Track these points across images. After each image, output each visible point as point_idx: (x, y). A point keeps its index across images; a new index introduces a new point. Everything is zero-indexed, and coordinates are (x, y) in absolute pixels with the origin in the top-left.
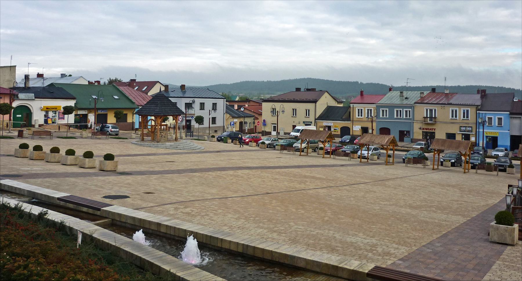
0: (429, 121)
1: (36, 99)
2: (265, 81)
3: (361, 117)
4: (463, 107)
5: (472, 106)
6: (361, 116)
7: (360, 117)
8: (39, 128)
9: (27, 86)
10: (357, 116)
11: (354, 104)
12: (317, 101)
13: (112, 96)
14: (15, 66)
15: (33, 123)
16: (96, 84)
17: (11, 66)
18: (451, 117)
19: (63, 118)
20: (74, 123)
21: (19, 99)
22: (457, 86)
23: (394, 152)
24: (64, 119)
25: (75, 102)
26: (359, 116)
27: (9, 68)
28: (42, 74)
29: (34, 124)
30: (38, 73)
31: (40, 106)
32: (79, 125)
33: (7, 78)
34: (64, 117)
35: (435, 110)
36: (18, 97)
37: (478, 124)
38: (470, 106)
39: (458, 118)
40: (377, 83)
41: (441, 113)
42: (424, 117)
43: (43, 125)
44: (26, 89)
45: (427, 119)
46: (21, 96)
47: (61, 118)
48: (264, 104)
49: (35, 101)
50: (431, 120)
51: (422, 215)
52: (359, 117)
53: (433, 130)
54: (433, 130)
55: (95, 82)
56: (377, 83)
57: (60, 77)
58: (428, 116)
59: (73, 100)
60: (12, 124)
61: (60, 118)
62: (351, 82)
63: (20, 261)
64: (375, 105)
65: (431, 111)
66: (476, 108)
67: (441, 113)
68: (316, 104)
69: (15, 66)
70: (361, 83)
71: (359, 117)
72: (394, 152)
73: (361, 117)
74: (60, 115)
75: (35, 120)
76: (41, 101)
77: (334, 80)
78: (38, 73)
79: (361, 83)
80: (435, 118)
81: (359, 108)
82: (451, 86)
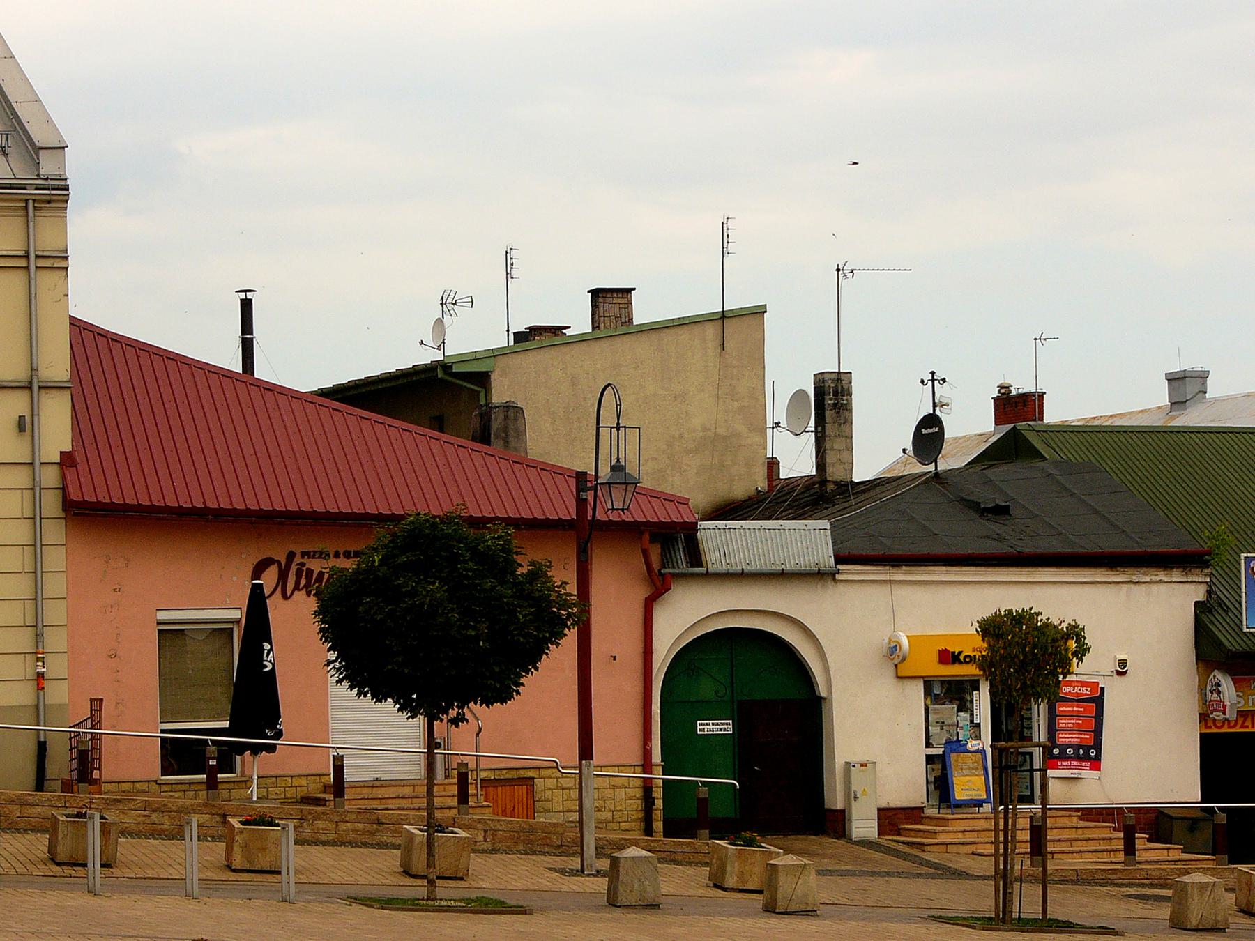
1: (850, 572)
8: (887, 840)
9: (835, 473)
14: (760, 311)
15: (835, 798)
17: (723, 316)
19: (1086, 758)
20: (1199, 800)
21: (708, 575)
23: (1037, 770)
24: (1096, 764)
25: (1199, 593)
27: (711, 331)
28: (1028, 388)
29: (840, 806)
30: (1004, 388)
31: (881, 638)
32: (1222, 819)
33: (697, 422)
34: (1098, 746)
36: (695, 556)
43: (914, 813)
47: (1077, 747)
49: (841, 588)
51: (555, 460)
57: (1166, 402)
59: (1176, 576)
60: (659, 803)
61: (1064, 748)
69: (760, 311)
72: (1037, 770)
74: (1062, 723)
75: (848, 766)
76: (886, 589)
78: (1004, 388)
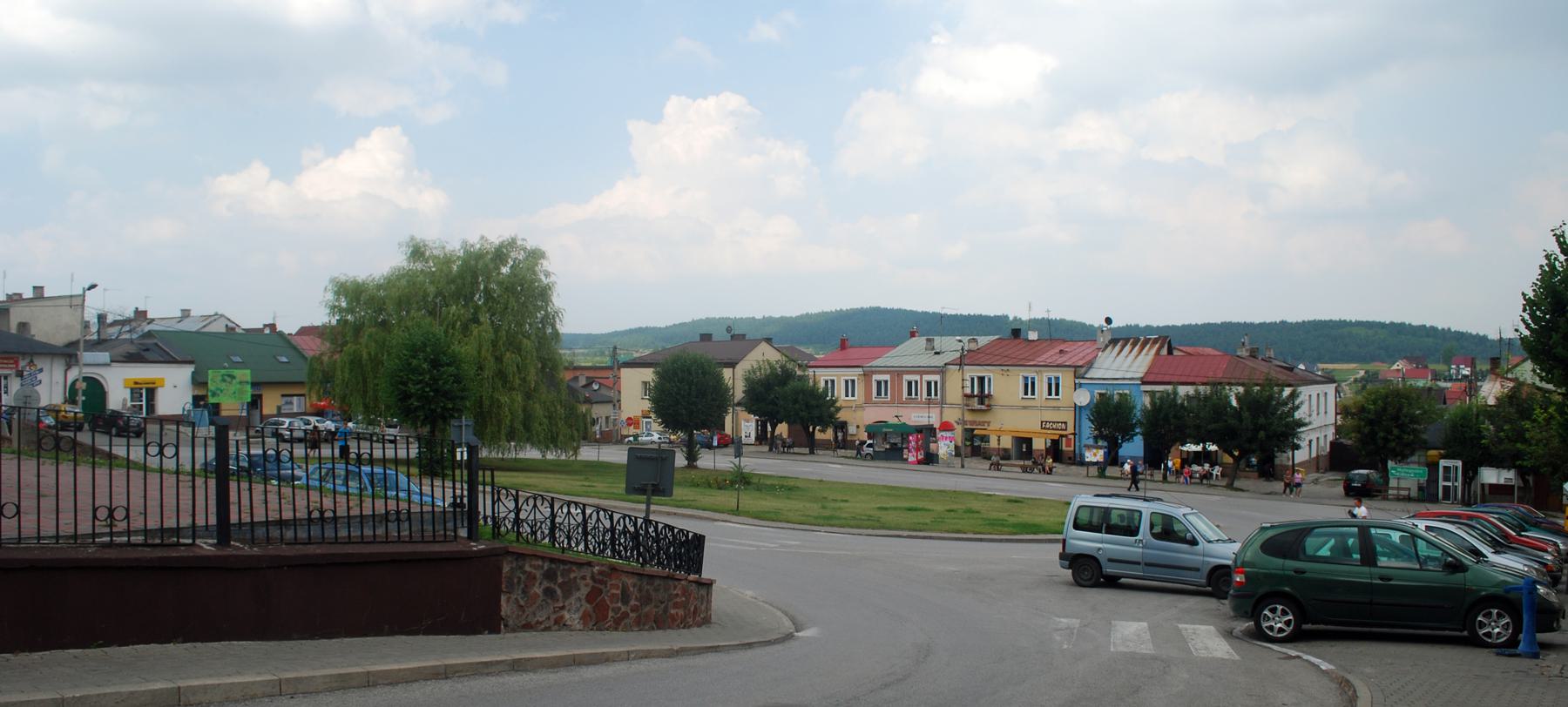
0: (976, 405)
2: (757, 317)
3: (853, 398)
4: (1048, 371)
5: (1065, 369)
6: (853, 395)
7: (850, 398)
10: (843, 396)
11: (816, 370)
12: (737, 364)
13: (274, 357)
16: (267, 331)
17: (71, 296)
18: (1021, 394)
22: (1278, 322)
25: (193, 370)
26: (847, 396)
35: (990, 380)
37: (1077, 410)
38: (1060, 369)
39: (919, 396)
40: (1354, 321)
41: (1005, 385)
42: (966, 396)
44: (99, 344)
45: (972, 399)
46: (87, 357)
48: (626, 373)
50: (982, 403)
52: (847, 398)
53: (986, 424)
54: (986, 424)
55: (265, 326)
56: (1354, 321)
58: (975, 393)
62: (987, 318)
63: (516, 599)
64: (861, 369)
65: (981, 379)
66: (1075, 372)
67: (1005, 385)
68: (736, 370)
70: (1015, 318)
71: (847, 398)
73: (853, 398)
77: (1293, 317)
79: (1015, 318)
80: (989, 396)
81: (846, 378)
82: (1260, 324)
